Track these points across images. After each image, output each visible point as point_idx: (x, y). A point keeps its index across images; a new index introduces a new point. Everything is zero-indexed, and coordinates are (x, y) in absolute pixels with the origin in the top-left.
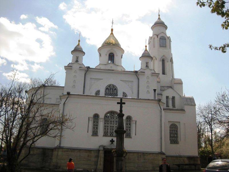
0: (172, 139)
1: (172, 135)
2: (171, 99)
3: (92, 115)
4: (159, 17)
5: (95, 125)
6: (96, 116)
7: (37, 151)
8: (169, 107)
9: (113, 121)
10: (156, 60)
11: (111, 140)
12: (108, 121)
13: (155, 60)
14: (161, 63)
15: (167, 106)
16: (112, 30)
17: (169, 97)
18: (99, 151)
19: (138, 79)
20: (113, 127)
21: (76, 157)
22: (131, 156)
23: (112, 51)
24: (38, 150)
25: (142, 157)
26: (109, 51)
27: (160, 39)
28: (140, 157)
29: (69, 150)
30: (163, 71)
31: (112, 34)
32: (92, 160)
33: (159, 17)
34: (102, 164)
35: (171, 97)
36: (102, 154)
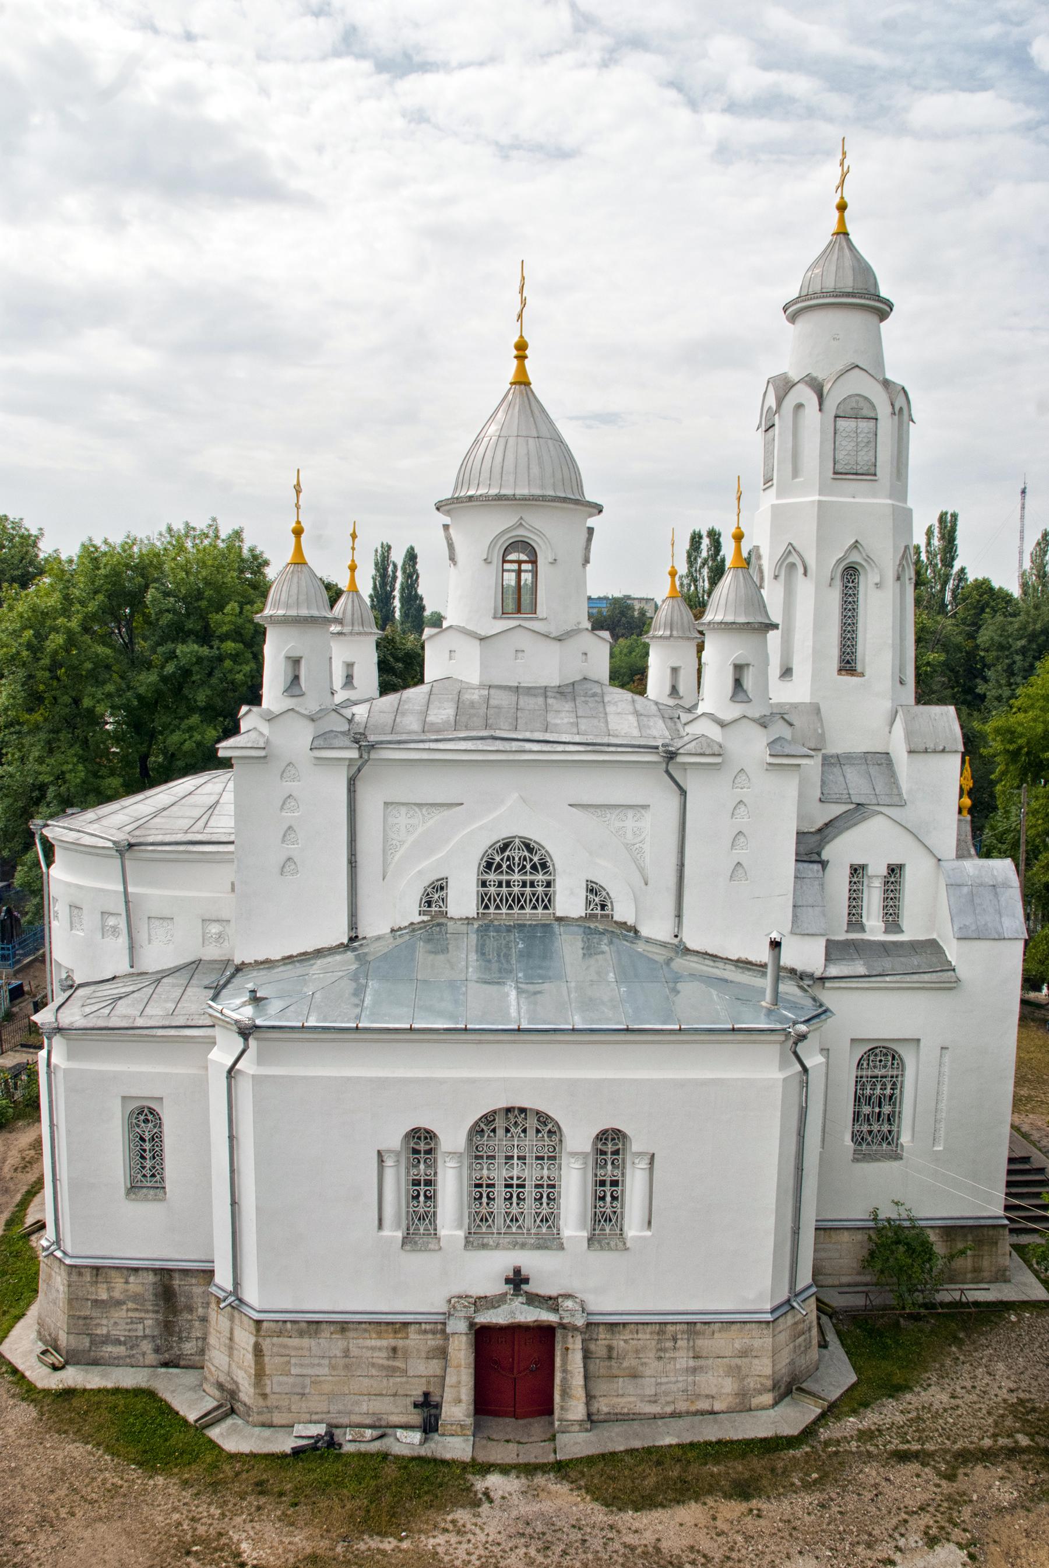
0: (865, 1128)
1: (866, 1110)
2: (878, 883)
3: (394, 1140)
4: (842, 221)
5: (416, 1183)
6: (421, 1143)
7: (127, 1282)
8: (862, 928)
9: (519, 1158)
10: (805, 574)
11: (511, 1275)
12: (493, 1186)
13: (801, 570)
14: (834, 597)
15: (855, 923)
16: (521, 347)
17: (871, 871)
18: (440, 1329)
19: (683, 792)
20: (523, 1186)
21: (326, 1362)
22: (622, 1343)
23: (521, 532)
24: (132, 1279)
25: (679, 1342)
26: (503, 533)
27: (836, 417)
28: (669, 1344)
29: (289, 1325)
30: (843, 638)
31: (522, 381)
32: (411, 1373)
33: (842, 221)
34: (464, 1397)
35: (878, 869)
36: (463, 1352)
